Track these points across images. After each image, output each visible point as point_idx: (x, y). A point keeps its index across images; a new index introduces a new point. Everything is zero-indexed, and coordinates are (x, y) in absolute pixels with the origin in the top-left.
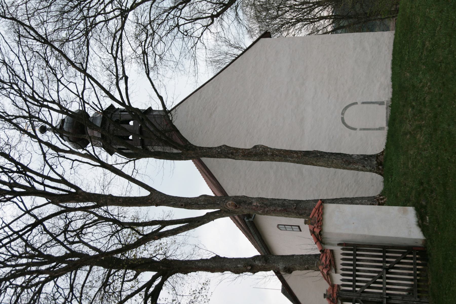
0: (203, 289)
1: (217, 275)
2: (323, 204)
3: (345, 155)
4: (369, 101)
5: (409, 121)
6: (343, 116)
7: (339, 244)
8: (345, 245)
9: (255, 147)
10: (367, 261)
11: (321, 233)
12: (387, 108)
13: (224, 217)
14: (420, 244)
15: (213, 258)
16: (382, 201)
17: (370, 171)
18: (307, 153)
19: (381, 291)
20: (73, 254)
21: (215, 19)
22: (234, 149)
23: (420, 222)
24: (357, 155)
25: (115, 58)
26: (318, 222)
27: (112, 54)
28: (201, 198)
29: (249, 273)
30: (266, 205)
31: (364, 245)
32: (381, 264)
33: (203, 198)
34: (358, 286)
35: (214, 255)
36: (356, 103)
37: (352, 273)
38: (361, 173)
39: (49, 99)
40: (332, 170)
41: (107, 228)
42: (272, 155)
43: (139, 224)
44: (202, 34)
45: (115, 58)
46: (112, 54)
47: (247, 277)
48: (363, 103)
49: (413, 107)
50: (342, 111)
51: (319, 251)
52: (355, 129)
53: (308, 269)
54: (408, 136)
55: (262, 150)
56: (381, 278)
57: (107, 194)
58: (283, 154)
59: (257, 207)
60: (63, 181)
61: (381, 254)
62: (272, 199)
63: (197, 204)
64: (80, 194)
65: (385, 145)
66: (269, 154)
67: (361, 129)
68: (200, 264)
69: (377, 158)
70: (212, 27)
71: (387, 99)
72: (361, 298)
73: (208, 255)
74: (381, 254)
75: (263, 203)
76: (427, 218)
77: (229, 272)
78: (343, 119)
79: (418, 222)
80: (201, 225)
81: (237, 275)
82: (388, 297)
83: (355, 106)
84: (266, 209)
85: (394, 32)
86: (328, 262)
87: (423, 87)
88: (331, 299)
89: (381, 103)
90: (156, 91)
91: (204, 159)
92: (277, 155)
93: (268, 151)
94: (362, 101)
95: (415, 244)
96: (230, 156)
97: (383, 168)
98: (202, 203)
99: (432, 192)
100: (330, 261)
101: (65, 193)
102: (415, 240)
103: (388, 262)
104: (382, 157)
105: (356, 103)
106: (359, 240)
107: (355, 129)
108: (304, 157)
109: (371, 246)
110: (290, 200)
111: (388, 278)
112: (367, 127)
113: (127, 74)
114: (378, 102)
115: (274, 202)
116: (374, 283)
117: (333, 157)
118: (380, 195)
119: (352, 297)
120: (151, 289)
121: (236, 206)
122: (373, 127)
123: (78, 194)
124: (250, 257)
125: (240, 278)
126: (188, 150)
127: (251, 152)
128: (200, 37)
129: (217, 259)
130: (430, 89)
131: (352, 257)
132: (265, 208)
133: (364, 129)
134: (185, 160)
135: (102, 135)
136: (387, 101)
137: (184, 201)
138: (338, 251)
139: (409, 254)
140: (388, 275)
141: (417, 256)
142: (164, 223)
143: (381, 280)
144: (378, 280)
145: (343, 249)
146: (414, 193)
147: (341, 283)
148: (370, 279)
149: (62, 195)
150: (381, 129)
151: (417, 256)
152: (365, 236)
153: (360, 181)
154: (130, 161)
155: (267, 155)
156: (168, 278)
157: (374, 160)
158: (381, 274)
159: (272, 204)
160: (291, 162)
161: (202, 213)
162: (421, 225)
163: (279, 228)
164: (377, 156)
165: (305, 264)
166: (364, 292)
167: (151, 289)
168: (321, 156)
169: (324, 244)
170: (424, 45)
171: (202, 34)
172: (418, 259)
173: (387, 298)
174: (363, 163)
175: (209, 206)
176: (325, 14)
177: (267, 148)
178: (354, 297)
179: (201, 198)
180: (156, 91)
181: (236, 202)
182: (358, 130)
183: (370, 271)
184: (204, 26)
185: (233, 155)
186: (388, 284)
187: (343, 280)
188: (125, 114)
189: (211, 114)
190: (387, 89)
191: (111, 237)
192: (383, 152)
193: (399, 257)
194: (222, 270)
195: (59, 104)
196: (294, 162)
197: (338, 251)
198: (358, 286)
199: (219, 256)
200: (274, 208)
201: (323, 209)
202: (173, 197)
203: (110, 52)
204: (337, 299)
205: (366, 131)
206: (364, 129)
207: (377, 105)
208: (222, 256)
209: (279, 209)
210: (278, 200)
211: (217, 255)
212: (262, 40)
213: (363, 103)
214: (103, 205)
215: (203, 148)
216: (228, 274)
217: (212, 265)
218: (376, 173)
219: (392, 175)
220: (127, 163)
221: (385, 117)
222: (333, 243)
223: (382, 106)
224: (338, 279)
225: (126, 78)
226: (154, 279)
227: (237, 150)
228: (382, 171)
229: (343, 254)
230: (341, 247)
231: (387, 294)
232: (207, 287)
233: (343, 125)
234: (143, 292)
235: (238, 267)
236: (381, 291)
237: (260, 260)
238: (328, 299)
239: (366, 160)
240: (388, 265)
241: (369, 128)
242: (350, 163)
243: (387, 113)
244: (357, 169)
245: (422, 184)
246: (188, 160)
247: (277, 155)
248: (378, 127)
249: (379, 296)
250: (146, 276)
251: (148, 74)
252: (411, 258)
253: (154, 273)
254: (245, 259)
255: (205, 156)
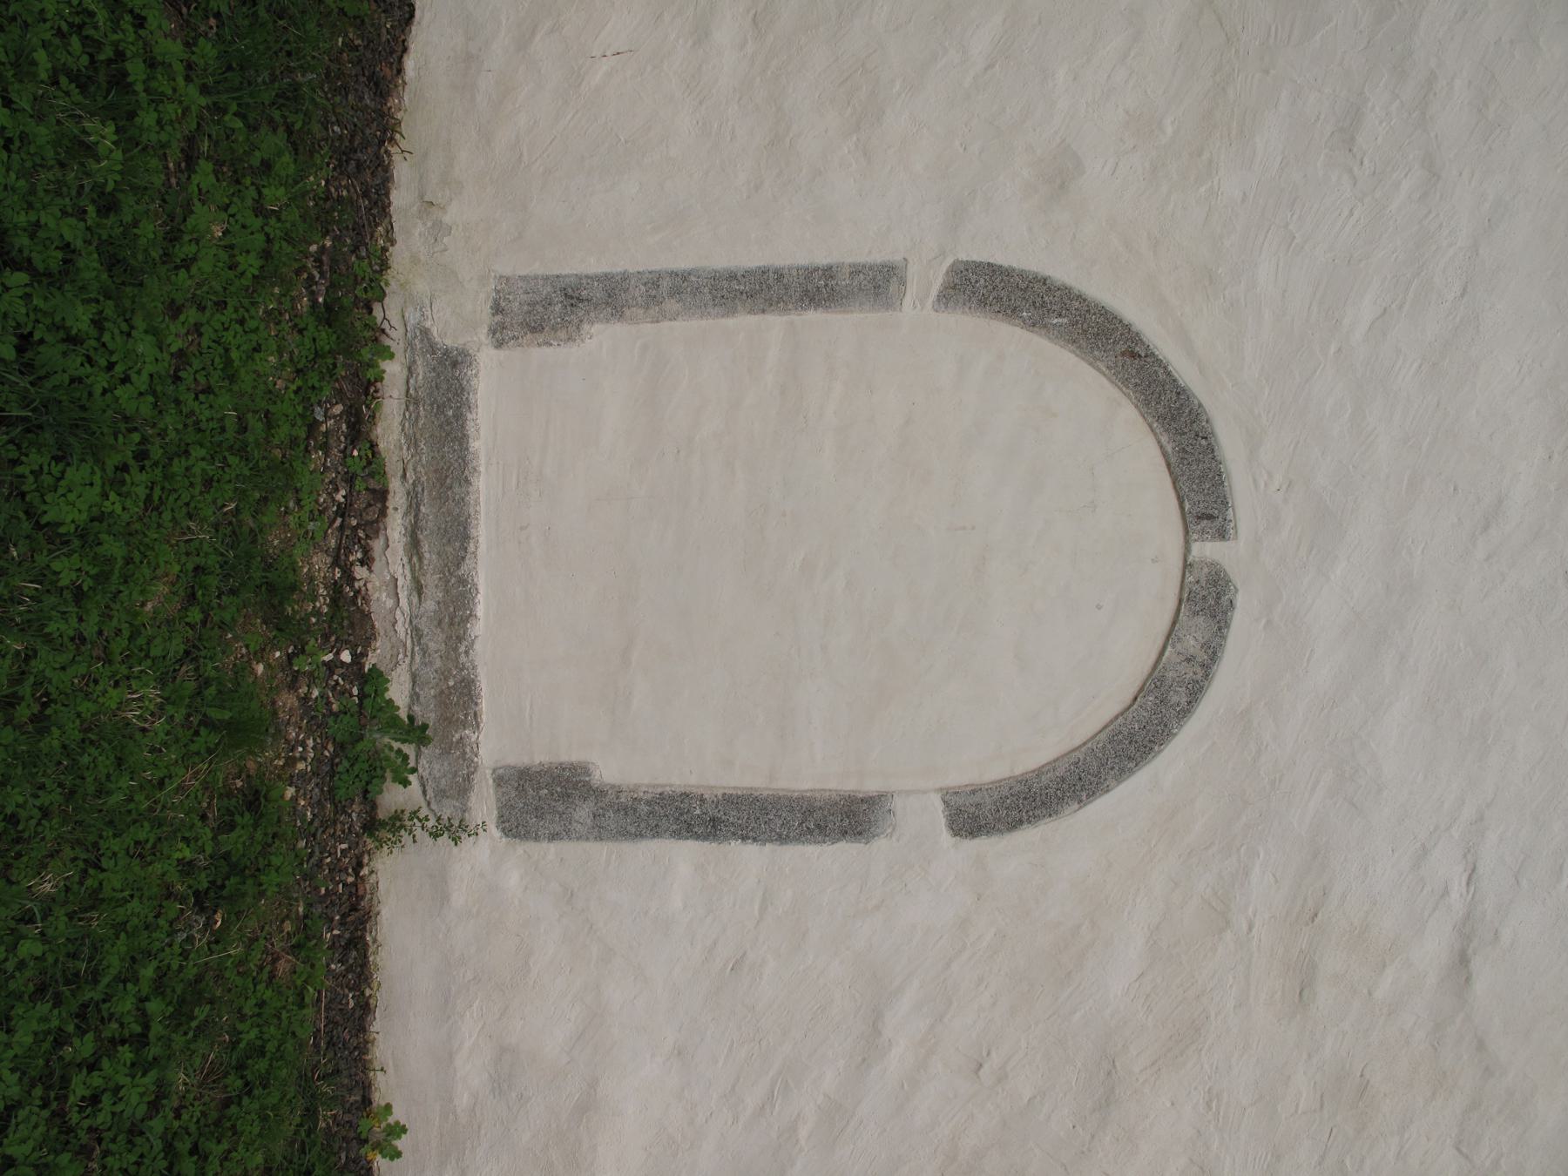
6: (1206, 550)
50: (1213, 653)
51: (388, 370)
65: (405, 50)
94: (880, 847)
112: (774, 325)
114: (599, 832)
136: (454, 830)
169: (78, 1153)
182: (924, 279)
188: (31, 582)
190: (472, 1073)
207: (609, 770)
221: (483, 532)
223: (539, 756)
233: (1185, 371)
241: (744, 322)
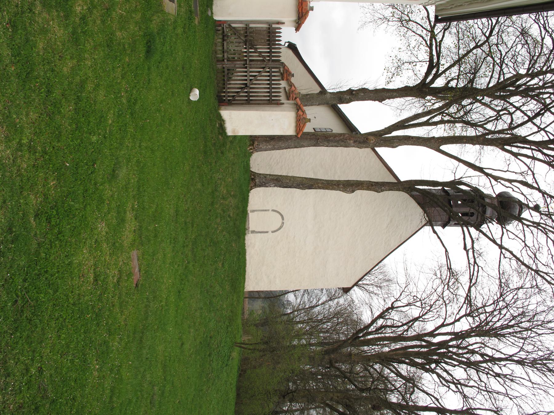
0: (391, 78)
1: (380, 87)
2: (296, 135)
3: (280, 187)
4: (262, 234)
5: (232, 206)
7: (283, 104)
8: (278, 103)
9: (353, 191)
10: (261, 92)
11: (297, 111)
12: (249, 228)
13: (377, 131)
14: (223, 107)
15: (384, 100)
16: (251, 147)
17: (260, 174)
18: (310, 187)
19: (251, 70)
20: (504, 98)
21: (390, 306)
22: (370, 190)
23: (222, 122)
24: (271, 187)
25: (475, 262)
26: (300, 120)
27: (478, 266)
28: (397, 145)
29: (353, 89)
30: (343, 141)
31: (264, 104)
32: (251, 90)
33: (395, 145)
34: (268, 72)
35: (383, 102)
36: (273, 232)
37: (273, 82)
38: (268, 173)
39: (532, 228)
40: (290, 175)
41: (474, 117)
42: (339, 185)
43: (448, 122)
44: (401, 295)
45: (475, 262)
46: (478, 266)
47: (355, 85)
48: (267, 232)
49: (229, 216)
52: (273, 211)
53: (307, 95)
54: (232, 193)
55: (347, 189)
56: (251, 80)
57: (477, 145)
58: (330, 186)
59: (350, 139)
60: (516, 155)
61: (251, 98)
62: (337, 147)
63: (399, 140)
64: (500, 144)
66: (341, 186)
67: (268, 210)
68: (395, 94)
69: (255, 184)
70: (393, 300)
71: (249, 235)
72: (265, 63)
73: (389, 102)
74: (251, 98)
75: (345, 142)
76: (217, 125)
77: (370, 89)
78: (283, 219)
79: (224, 124)
80: (396, 124)
81: (364, 87)
82: (246, 65)
83: (273, 230)
84: (342, 137)
85: (245, 290)
86: (291, 96)
87: (223, 231)
88: (288, 73)
89: (253, 232)
90: (439, 238)
91: (396, 181)
92: (335, 185)
93: (342, 188)
95: (226, 107)
96: (374, 184)
97: (251, 176)
98: (395, 141)
99: (215, 144)
100: (290, 96)
101: (515, 144)
102: (226, 110)
103: (246, 92)
104: (252, 185)
105: (273, 232)
106: (267, 107)
107: (273, 211)
108: (313, 183)
109: (259, 104)
110: (323, 146)
111: (246, 80)
113: (465, 252)
115: (336, 144)
116: (256, 76)
117: (290, 184)
118: (252, 153)
119: (272, 63)
120: (434, 72)
121: (367, 139)
122: (259, 212)
123: (502, 144)
124: (354, 102)
125: (361, 84)
126: (409, 188)
127: (356, 187)
128: (402, 292)
129: (381, 100)
130: (218, 227)
131: (273, 94)
132: (343, 138)
133: (266, 210)
134: (412, 180)
135: (484, 200)
137: (410, 141)
138: (283, 99)
139: (230, 100)
140: (246, 82)
141: (224, 98)
142: (427, 123)
143: (251, 78)
144: (253, 78)
145: (280, 100)
146: (228, 147)
147: (281, 82)
148: (259, 78)
149: (516, 143)
150: (253, 211)
151: (224, 98)
152: (263, 110)
153: (268, 168)
154: (459, 179)
155: (343, 185)
156: (421, 82)
157: (258, 183)
158: (251, 83)
159: (338, 141)
160: (323, 180)
161: (395, 134)
162: (221, 122)
163: (331, 130)
164: (256, 186)
165: (309, 98)
166: (263, 68)
167: (434, 72)
168: (299, 185)
169: (295, 104)
170: (223, 264)
171: (401, 295)
172: (224, 96)
173: (246, 64)
174: (266, 180)
175: (389, 139)
176: (300, 326)
177: (343, 191)
178: (270, 63)
179: (397, 145)
180: (439, 238)
181: (367, 143)
183: (259, 84)
184: (399, 301)
185: (371, 184)
186: (246, 76)
187: (280, 84)
189: (391, 221)
190: (249, 243)
191: (472, 109)
192: (251, 189)
193: (238, 97)
194: (376, 91)
195: (523, 224)
196: (321, 180)
197: (283, 99)
198: (268, 72)
199: (379, 102)
200: (336, 139)
201: (296, 130)
202: (420, 145)
203: (480, 268)
204: (284, 73)
205: (265, 209)
206: (266, 210)
208: (377, 102)
209: (332, 138)
210: (332, 146)
211: (381, 102)
212: (350, 286)
213: (267, 232)
214: (480, 136)
215: (397, 190)
216: (371, 87)
217: (384, 94)
218: (256, 173)
219: (244, 166)
220: (461, 178)
222: (288, 105)
224: (283, 84)
225: (465, 248)
226: (433, 81)
227: (368, 189)
228: (251, 174)
229: (279, 96)
230: (281, 102)
231: (246, 68)
232: (388, 80)
234: (441, 69)
235: (363, 93)
236: (251, 70)
237: (345, 99)
238: (290, 73)
239: (264, 183)
240: (246, 90)
242: (276, 180)
243: (249, 224)
244: (270, 175)
245: (222, 153)
246: (410, 180)
247: (335, 185)
248: (255, 212)
249: (252, 66)
250: (440, 83)
251: (446, 251)
252: (229, 96)
253: (432, 86)
254: (358, 100)
255: (395, 183)
